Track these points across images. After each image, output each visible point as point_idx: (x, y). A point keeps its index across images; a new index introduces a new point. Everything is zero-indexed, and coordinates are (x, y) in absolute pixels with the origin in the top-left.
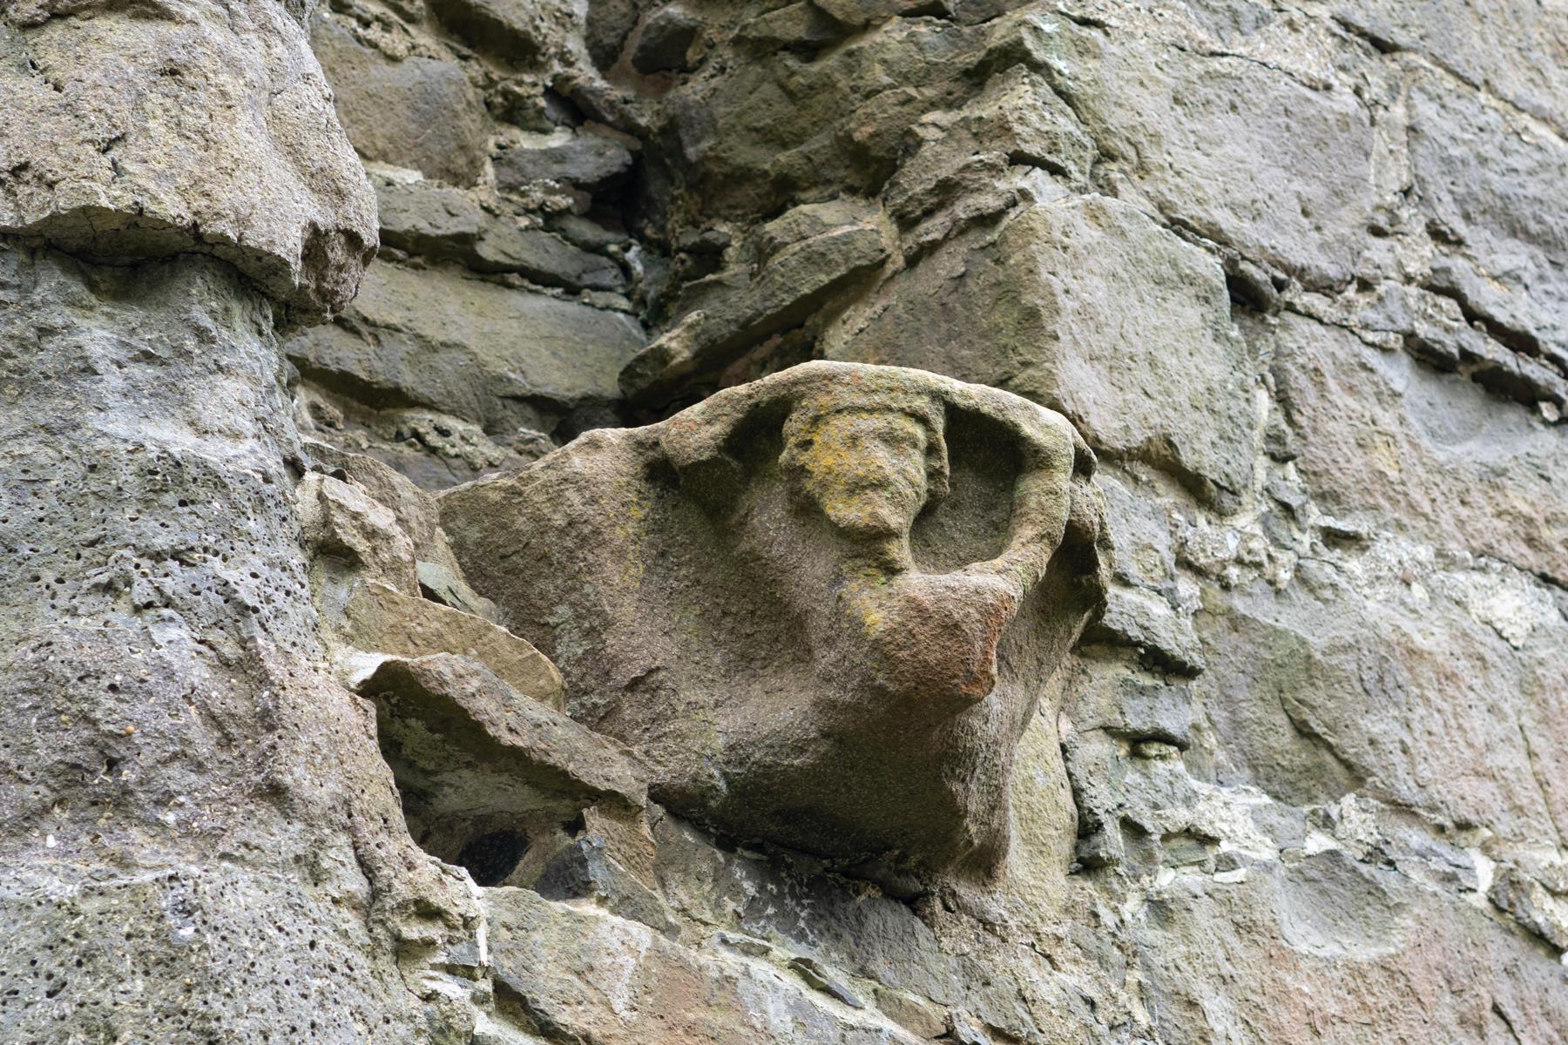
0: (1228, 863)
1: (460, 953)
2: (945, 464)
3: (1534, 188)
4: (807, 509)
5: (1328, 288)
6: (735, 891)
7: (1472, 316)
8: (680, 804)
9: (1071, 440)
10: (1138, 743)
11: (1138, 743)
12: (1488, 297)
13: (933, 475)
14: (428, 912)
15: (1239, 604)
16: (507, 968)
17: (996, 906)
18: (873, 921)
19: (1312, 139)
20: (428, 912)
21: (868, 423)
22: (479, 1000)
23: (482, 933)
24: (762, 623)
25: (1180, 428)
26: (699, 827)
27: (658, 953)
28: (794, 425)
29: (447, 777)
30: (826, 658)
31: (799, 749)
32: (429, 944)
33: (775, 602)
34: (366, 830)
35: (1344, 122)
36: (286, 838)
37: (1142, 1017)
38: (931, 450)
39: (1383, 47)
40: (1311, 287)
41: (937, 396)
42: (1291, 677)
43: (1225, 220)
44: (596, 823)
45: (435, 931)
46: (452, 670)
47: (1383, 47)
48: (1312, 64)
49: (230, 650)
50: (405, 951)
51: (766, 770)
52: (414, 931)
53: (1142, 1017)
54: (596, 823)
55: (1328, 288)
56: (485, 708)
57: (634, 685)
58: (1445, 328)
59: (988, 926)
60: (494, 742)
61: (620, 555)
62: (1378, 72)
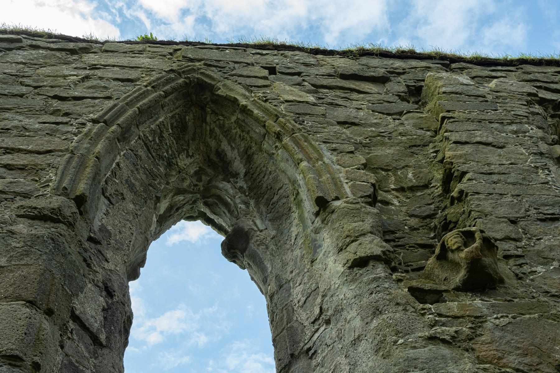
0: (540, 273)
1: (430, 312)
2: (463, 237)
3: (546, 201)
4: (452, 251)
5: (523, 218)
6: (469, 296)
7: (545, 214)
8: (457, 289)
9: (486, 232)
10: (520, 265)
11: (520, 265)
12: (546, 212)
13: (463, 239)
14: (423, 309)
15: (528, 249)
16: (438, 312)
17: (506, 285)
18: (489, 292)
19: (512, 205)
20: (423, 309)
21: (451, 238)
22: (436, 316)
23: (433, 309)
24: (456, 265)
25: (509, 235)
26: (461, 291)
27: (458, 304)
28: (446, 243)
29: (426, 298)
30: (462, 264)
31: (465, 276)
32: (425, 313)
33: (456, 263)
34: (412, 304)
35: (517, 203)
36: (401, 308)
37: (534, 291)
38: (461, 237)
39: (519, 196)
40: (521, 218)
41: (458, 231)
42: (539, 253)
43: (505, 216)
44: (444, 294)
45: (426, 311)
46: (414, 284)
47: (519, 196)
48: (510, 200)
49: (387, 293)
50: (423, 315)
51: (464, 280)
52: (422, 312)
53: (534, 291)
54: (444, 294)
55: (523, 218)
56: (423, 287)
57: (445, 280)
58: (541, 216)
59: (506, 288)
60: (426, 290)
61: (437, 268)
62: (519, 198)
